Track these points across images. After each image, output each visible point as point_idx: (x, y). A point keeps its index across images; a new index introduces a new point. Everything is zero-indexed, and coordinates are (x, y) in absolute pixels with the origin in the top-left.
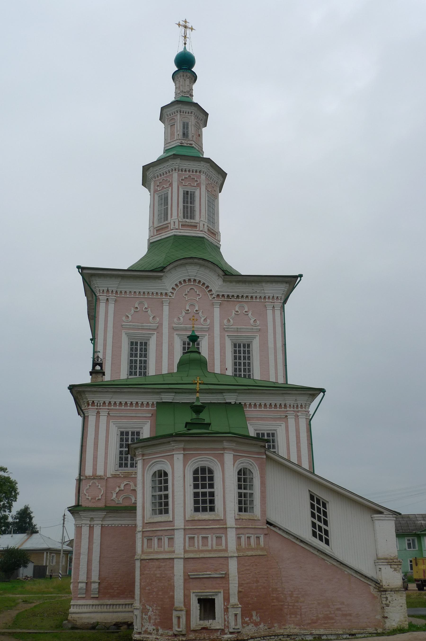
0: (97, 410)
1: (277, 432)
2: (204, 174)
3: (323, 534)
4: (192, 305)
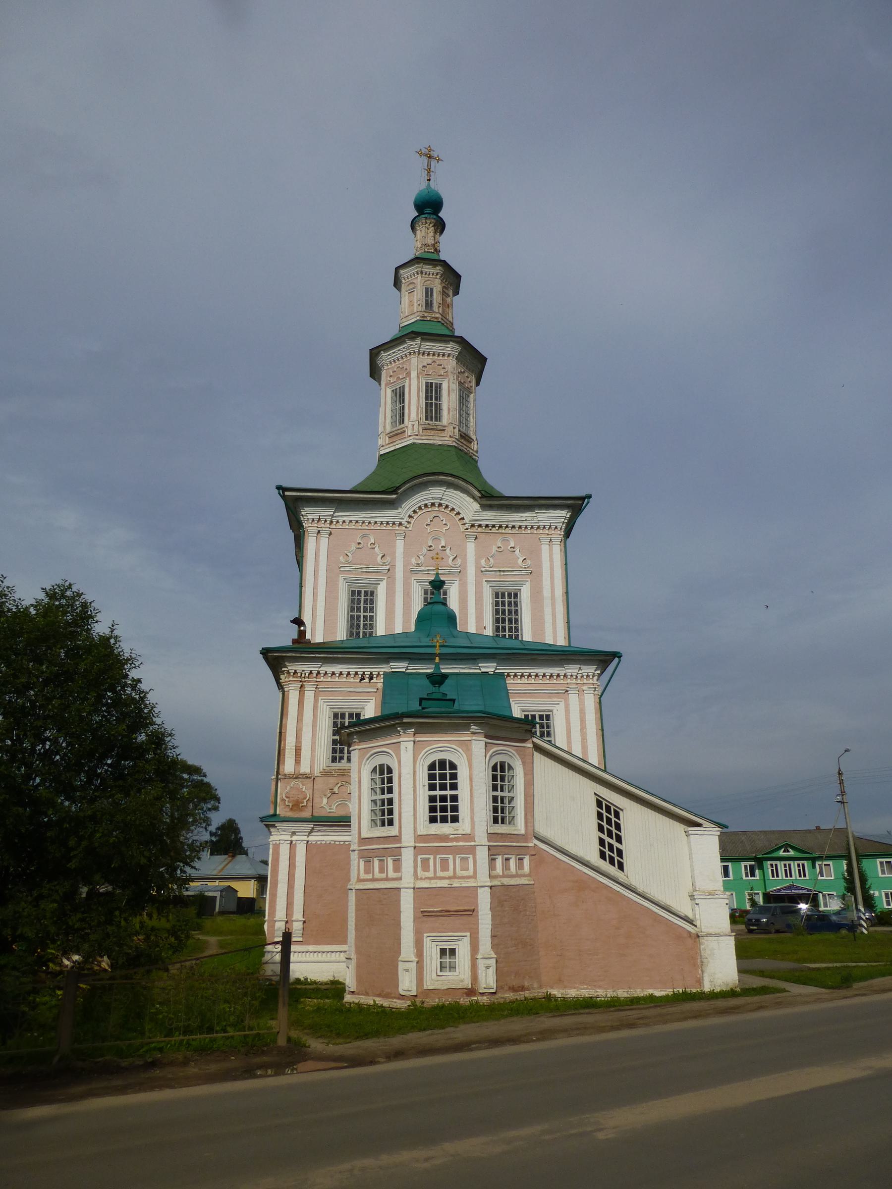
0: (301, 683)
1: (553, 713)
2: (454, 359)
3: (608, 853)
4: (436, 539)
